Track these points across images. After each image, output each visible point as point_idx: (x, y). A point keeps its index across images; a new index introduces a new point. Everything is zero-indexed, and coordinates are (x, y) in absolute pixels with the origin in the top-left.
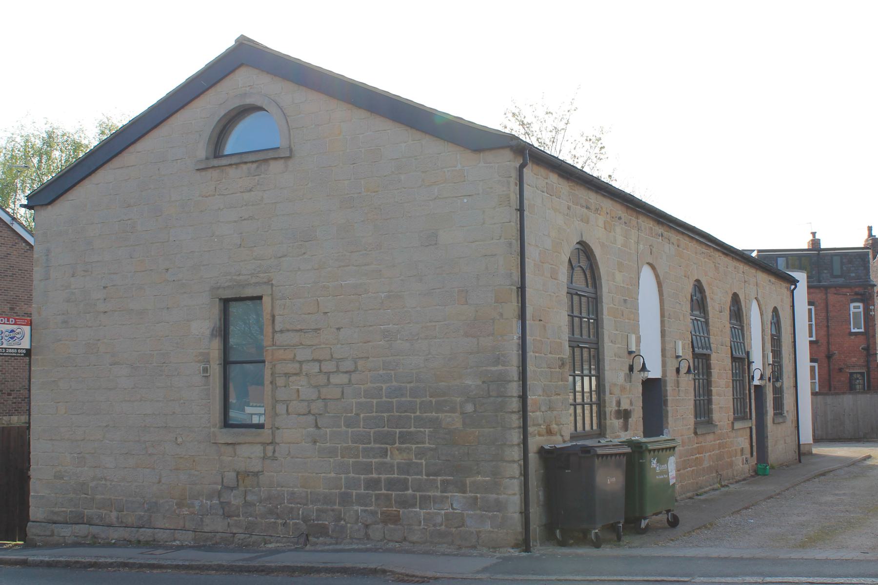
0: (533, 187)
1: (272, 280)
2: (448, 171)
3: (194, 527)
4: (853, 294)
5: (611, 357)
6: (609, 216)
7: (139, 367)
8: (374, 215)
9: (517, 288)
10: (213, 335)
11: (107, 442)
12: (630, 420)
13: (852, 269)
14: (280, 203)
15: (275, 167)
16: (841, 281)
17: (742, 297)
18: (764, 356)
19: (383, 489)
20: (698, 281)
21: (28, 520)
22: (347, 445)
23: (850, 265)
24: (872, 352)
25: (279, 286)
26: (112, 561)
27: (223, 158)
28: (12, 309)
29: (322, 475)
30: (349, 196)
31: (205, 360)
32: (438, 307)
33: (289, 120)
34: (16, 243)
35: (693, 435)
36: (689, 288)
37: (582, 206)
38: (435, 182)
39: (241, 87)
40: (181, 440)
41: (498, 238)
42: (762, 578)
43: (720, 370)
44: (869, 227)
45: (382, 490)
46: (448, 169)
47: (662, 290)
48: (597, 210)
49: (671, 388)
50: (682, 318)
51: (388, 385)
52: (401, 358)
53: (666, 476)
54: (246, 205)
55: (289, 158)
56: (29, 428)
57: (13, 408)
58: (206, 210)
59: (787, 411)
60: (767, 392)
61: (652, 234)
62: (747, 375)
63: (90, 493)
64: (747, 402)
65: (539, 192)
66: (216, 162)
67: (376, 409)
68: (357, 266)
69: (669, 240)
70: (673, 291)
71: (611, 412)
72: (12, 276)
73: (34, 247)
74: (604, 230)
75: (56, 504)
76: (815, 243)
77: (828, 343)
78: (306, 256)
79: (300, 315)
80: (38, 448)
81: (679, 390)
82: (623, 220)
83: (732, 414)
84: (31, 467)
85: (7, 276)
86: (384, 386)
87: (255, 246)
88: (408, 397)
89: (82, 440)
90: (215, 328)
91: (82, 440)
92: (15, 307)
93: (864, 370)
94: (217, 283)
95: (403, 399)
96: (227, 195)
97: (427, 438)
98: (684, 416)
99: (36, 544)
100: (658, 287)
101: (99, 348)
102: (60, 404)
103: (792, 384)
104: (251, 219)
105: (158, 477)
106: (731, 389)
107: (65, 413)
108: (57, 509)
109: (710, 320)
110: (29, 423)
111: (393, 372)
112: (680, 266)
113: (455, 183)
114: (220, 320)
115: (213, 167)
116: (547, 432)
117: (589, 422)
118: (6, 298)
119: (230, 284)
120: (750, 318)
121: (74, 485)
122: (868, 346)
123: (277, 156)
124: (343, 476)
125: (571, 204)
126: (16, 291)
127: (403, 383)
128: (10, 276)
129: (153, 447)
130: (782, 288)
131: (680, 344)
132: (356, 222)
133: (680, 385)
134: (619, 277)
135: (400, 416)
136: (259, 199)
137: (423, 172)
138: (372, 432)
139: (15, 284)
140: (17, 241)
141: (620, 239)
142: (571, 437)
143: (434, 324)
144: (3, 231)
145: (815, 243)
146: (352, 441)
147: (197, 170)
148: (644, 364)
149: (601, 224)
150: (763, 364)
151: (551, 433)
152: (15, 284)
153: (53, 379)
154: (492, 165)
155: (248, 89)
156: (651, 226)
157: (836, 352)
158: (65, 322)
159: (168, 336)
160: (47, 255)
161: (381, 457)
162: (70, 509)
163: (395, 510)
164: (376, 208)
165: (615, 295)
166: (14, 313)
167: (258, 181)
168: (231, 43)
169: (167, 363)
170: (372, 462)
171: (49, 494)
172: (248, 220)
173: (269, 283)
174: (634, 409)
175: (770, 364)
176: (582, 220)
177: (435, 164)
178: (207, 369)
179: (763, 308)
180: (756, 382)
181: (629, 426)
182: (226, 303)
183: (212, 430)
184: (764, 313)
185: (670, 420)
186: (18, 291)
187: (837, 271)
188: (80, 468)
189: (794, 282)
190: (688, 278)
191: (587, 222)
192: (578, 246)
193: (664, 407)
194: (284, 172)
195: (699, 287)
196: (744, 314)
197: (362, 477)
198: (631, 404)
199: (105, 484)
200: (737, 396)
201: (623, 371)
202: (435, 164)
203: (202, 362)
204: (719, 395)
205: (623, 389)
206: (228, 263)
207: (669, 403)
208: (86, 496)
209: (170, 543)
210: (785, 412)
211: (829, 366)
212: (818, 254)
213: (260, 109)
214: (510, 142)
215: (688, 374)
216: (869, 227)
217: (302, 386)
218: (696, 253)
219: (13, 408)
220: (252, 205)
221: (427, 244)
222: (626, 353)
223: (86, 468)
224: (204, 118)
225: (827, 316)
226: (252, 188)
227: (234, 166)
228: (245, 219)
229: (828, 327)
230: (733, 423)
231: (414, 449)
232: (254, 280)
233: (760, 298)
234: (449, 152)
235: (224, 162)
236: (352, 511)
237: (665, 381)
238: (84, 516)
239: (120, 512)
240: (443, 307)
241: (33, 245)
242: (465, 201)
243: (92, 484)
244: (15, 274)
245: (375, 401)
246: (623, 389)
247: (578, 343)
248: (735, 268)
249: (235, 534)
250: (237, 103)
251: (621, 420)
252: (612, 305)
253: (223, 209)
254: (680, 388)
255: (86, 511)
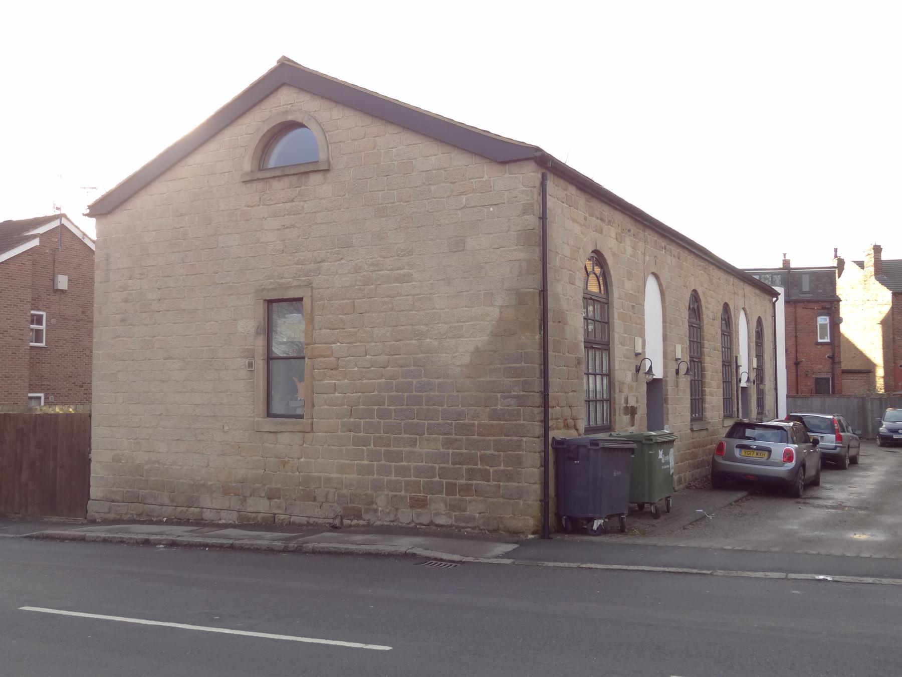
0: (555, 198)
1: (312, 283)
2: (475, 182)
3: (238, 508)
4: (820, 308)
5: (620, 358)
6: (620, 228)
7: (190, 361)
8: (406, 223)
9: (540, 291)
10: (257, 333)
11: (161, 429)
12: (636, 416)
13: (820, 285)
14: (319, 212)
15: (315, 179)
16: (809, 296)
17: (731, 307)
18: (750, 361)
19: (412, 476)
20: (695, 291)
21: (89, 499)
22: (379, 435)
23: (818, 283)
24: (836, 360)
25: (319, 289)
26: (162, 538)
27: (266, 171)
28: (83, 312)
29: (356, 462)
30: (382, 206)
31: (251, 356)
32: (465, 309)
33: (327, 135)
34: (87, 255)
35: (689, 431)
36: (687, 296)
37: (597, 218)
38: (463, 192)
39: (283, 105)
40: (228, 428)
41: (522, 244)
42: (785, 574)
43: (712, 372)
44: (835, 249)
45: (411, 477)
46: (476, 180)
47: (664, 298)
48: (610, 221)
49: (671, 388)
50: (681, 324)
51: (418, 380)
52: (431, 355)
53: (668, 466)
54: (287, 214)
55: (327, 170)
56: (90, 416)
57: (84, 398)
58: (251, 218)
59: (768, 411)
60: (752, 393)
61: (656, 246)
62: (735, 377)
63: (145, 475)
64: (735, 402)
65: (560, 202)
66: (260, 175)
67: (407, 402)
68: (390, 270)
69: (671, 252)
70: (674, 299)
71: (620, 409)
72: (83, 284)
73: (95, 253)
74: (615, 240)
75: (114, 484)
76: (786, 263)
77: (796, 351)
78: (343, 261)
79: (338, 315)
80: (99, 434)
81: (678, 390)
82: (632, 232)
83: (723, 412)
84: (92, 451)
85: (79, 283)
86: (415, 382)
87: (296, 252)
88: (436, 392)
89: (138, 427)
90: (260, 327)
91: (138, 427)
92: (86, 310)
93: (829, 376)
94: (262, 286)
95: (432, 394)
96: (271, 205)
97: (454, 429)
98: (682, 414)
99: (96, 520)
100: (661, 295)
101: (154, 344)
102: (118, 394)
103: (773, 387)
104: (293, 228)
105: (206, 461)
106: (722, 390)
107: (123, 403)
108: (115, 489)
109: (704, 327)
110: (91, 411)
111: (422, 369)
112: (680, 277)
113: (481, 193)
114: (264, 319)
115: (258, 179)
116: (564, 426)
117: (599, 415)
118: (78, 302)
119: (273, 287)
120: (738, 326)
121: (131, 468)
122: (833, 355)
123: (316, 169)
124: (375, 463)
125: (587, 215)
126: (87, 297)
127: (432, 378)
128: (82, 284)
129: (202, 434)
130: (765, 300)
131: (679, 349)
132: (389, 230)
133: (679, 385)
134: (628, 285)
135: (429, 409)
136: (300, 208)
137: (452, 183)
138: (402, 423)
139: (86, 291)
140: (88, 253)
141: (629, 250)
142: (585, 431)
143: (461, 324)
144: (76, 244)
145: (786, 263)
146: (384, 431)
147: (244, 182)
148: (651, 368)
149: (613, 235)
150: (749, 368)
151: (568, 427)
152: (86, 291)
153: (112, 372)
154: (516, 175)
155: (289, 107)
156: (656, 239)
157: (804, 360)
158: (123, 320)
159: (216, 334)
160: (107, 260)
161: (411, 446)
162: (127, 490)
163: (423, 496)
164: (407, 217)
165: (625, 301)
166: (86, 316)
167: (299, 192)
168: (273, 64)
169: (216, 358)
170: (402, 451)
171: (108, 475)
172: (290, 228)
173: (309, 285)
174: (639, 406)
175: (755, 368)
176: (596, 231)
177: (464, 175)
178: (252, 364)
179: (749, 317)
180: (743, 384)
181: (635, 421)
182: (270, 302)
183: (256, 419)
184: (750, 320)
185: (670, 417)
186: (89, 297)
187: (806, 288)
188: (136, 453)
189: (776, 294)
190: (687, 288)
191: (601, 233)
192: (593, 255)
193: (664, 405)
194: (323, 184)
195: (695, 297)
196: (734, 323)
197: (393, 464)
198: (637, 401)
199: (159, 467)
200: (726, 396)
201: (631, 371)
202: (464, 175)
203: (247, 358)
204: (711, 395)
205: (631, 388)
206: (271, 267)
207: (670, 402)
208: (140, 477)
209: (216, 522)
210: (766, 412)
211: (797, 372)
212: (789, 273)
213: (300, 125)
214: (535, 154)
215: (686, 376)
216: (835, 249)
217: (338, 380)
218: (694, 265)
219: (84, 398)
220: (294, 214)
221: (455, 250)
222: (634, 355)
223: (141, 453)
224: (249, 134)
225: (796, 327)
226: (294, 198)
227: (277, 178)
228: (287, 228)
229: (796, 337)
230: (723, 421)
231: (441, 440)
232: (295, 283)
233: (747, 308)
234: (476, 164)
235: (268, 175)
236: (383, 496)
237: (666, 381)
238: (139, 496)
239: (171, 492)
240: (470, 309)
241: (94, 250)
242: (492, 209)
243: (146, 467)
244: (86, 282)
245: (405, 395)
246: (631, 388)
247: (592, 344)
248: (726, 281)
249: (276, 514)
250: (280, 119)
251: (629, 416)
252: (622, 310)
253: (267, 217)
254: (679, 388)
255: (140, 491)
